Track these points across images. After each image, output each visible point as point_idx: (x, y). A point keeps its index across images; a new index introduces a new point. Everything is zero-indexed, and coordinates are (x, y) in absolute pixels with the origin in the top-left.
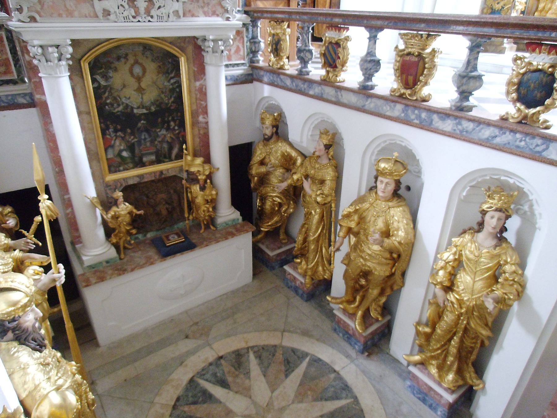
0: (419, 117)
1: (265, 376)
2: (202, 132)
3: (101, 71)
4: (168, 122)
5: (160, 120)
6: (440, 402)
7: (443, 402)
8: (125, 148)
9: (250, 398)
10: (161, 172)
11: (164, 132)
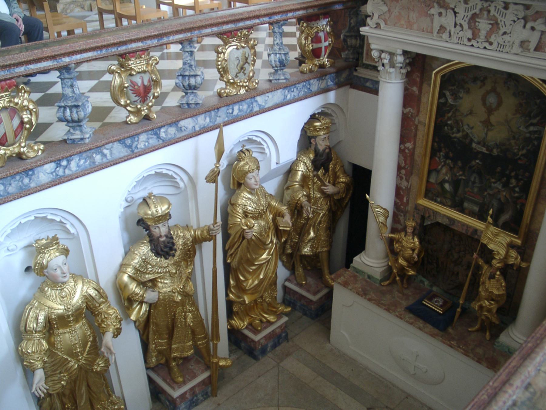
3: (453, 88)
5: (499, 169)
11: (499, 186)
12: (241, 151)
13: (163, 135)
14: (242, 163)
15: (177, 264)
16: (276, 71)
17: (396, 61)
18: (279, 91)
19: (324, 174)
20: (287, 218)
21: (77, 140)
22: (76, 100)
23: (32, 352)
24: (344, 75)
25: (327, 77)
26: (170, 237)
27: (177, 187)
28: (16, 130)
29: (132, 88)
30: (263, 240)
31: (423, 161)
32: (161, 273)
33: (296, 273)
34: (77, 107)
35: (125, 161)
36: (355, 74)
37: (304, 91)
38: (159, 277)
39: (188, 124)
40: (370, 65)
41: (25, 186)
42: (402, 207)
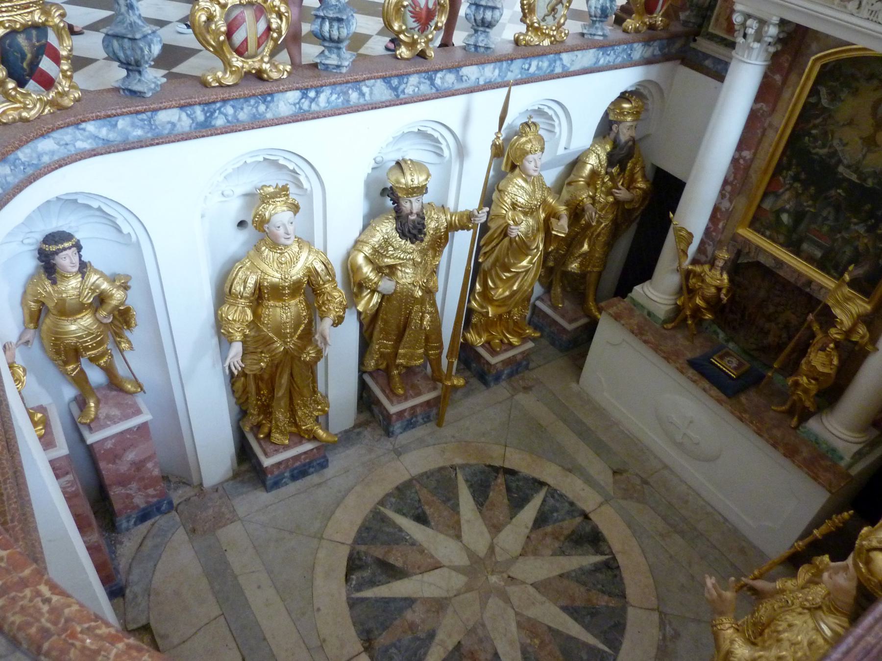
1: (561, 576)
3: (834, 84)
5: (868, 207)
8: (792, 210)
10: (810, 282)
11: (861, 229)
12: (526, 123)
13: (438, 81)
14: (524, 139)
15: (423, 253)
16: (594, 22)
17: (767, 32)
18: (592, 51)
19: (619, 174)
20: (564, 222)
21: (331, 67)
22: (340, 11)
23: (234, 320)
24: (678, 45)
25: (656, 44)
26: (421, 216)
27: (440, 155)
28: (260, 37)
29: (411, 9)
30: (529, 244)
31: (759, 180)
32: (403, 259)
33: (552, 292)
34: (340, 20)
35: (387, 106)
36: (693, 45)
37: (623, 58)
38: (400, 264)
39: (471, 73)
40: (717, 36)
41: (260, 115)
42: (714, 234)
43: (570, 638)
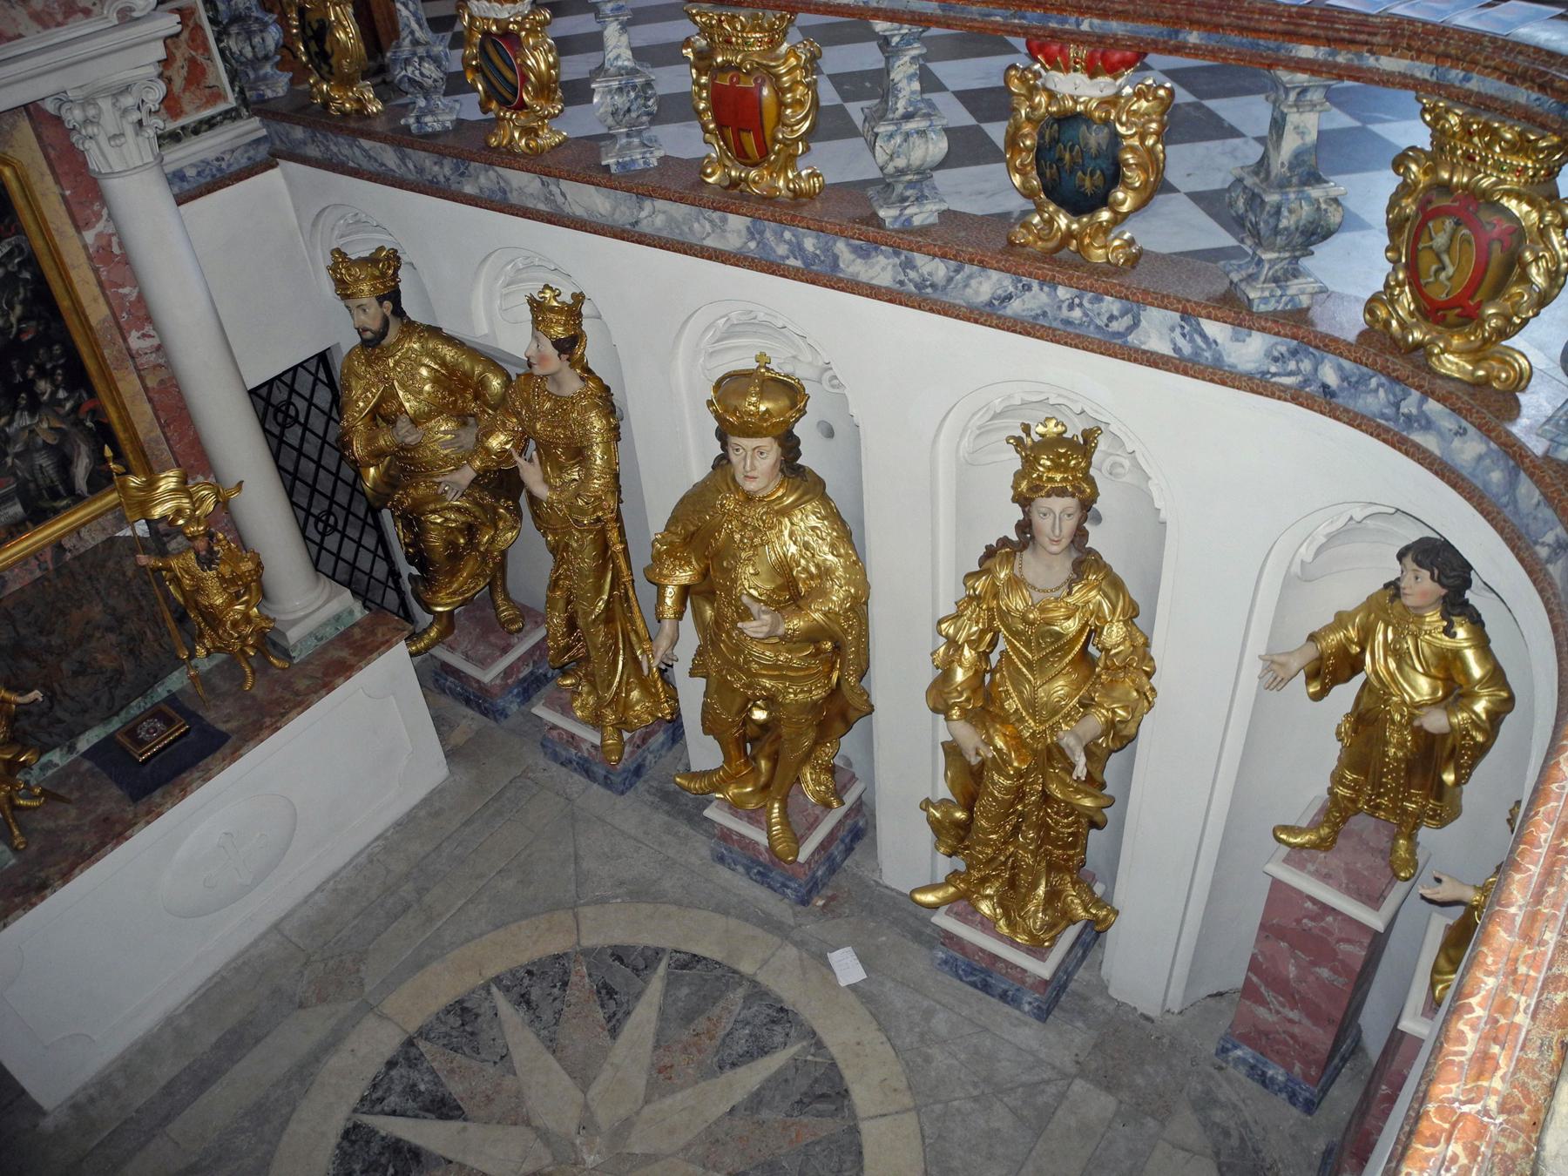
0: (797, 249)
2: (152, 382)
4: (29, 385)
6: (1024, 983)
7: (1029, 981)
9: (528, 1123)
11: (23, 420)
43: (663, 1016)
